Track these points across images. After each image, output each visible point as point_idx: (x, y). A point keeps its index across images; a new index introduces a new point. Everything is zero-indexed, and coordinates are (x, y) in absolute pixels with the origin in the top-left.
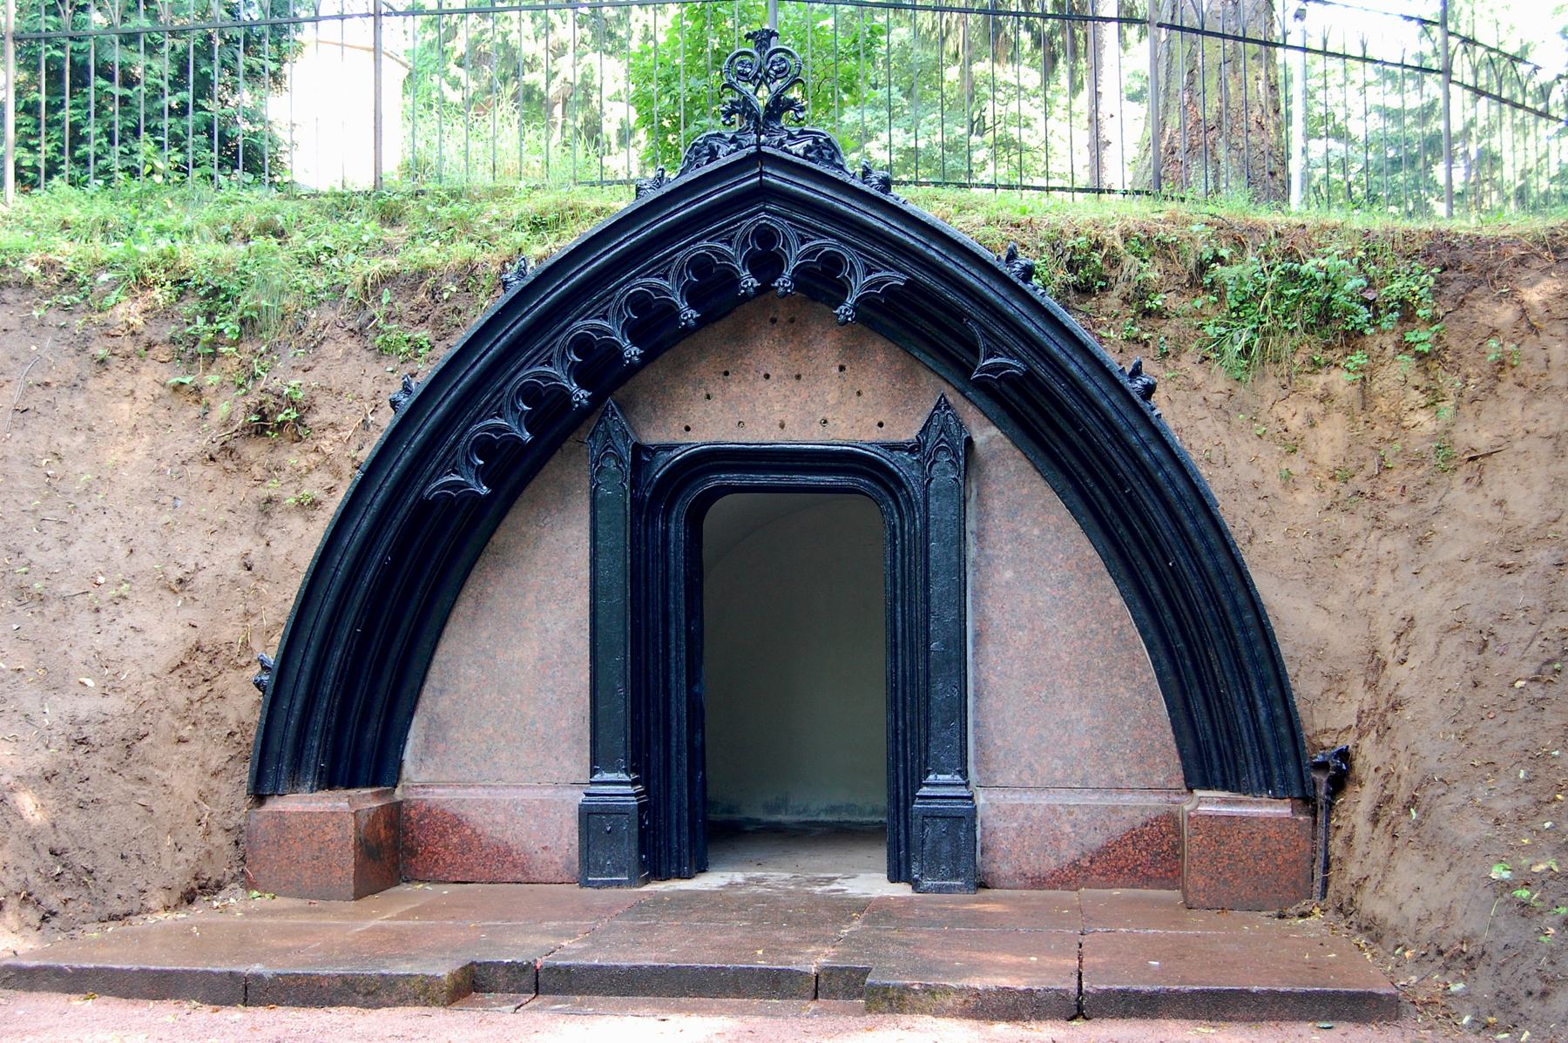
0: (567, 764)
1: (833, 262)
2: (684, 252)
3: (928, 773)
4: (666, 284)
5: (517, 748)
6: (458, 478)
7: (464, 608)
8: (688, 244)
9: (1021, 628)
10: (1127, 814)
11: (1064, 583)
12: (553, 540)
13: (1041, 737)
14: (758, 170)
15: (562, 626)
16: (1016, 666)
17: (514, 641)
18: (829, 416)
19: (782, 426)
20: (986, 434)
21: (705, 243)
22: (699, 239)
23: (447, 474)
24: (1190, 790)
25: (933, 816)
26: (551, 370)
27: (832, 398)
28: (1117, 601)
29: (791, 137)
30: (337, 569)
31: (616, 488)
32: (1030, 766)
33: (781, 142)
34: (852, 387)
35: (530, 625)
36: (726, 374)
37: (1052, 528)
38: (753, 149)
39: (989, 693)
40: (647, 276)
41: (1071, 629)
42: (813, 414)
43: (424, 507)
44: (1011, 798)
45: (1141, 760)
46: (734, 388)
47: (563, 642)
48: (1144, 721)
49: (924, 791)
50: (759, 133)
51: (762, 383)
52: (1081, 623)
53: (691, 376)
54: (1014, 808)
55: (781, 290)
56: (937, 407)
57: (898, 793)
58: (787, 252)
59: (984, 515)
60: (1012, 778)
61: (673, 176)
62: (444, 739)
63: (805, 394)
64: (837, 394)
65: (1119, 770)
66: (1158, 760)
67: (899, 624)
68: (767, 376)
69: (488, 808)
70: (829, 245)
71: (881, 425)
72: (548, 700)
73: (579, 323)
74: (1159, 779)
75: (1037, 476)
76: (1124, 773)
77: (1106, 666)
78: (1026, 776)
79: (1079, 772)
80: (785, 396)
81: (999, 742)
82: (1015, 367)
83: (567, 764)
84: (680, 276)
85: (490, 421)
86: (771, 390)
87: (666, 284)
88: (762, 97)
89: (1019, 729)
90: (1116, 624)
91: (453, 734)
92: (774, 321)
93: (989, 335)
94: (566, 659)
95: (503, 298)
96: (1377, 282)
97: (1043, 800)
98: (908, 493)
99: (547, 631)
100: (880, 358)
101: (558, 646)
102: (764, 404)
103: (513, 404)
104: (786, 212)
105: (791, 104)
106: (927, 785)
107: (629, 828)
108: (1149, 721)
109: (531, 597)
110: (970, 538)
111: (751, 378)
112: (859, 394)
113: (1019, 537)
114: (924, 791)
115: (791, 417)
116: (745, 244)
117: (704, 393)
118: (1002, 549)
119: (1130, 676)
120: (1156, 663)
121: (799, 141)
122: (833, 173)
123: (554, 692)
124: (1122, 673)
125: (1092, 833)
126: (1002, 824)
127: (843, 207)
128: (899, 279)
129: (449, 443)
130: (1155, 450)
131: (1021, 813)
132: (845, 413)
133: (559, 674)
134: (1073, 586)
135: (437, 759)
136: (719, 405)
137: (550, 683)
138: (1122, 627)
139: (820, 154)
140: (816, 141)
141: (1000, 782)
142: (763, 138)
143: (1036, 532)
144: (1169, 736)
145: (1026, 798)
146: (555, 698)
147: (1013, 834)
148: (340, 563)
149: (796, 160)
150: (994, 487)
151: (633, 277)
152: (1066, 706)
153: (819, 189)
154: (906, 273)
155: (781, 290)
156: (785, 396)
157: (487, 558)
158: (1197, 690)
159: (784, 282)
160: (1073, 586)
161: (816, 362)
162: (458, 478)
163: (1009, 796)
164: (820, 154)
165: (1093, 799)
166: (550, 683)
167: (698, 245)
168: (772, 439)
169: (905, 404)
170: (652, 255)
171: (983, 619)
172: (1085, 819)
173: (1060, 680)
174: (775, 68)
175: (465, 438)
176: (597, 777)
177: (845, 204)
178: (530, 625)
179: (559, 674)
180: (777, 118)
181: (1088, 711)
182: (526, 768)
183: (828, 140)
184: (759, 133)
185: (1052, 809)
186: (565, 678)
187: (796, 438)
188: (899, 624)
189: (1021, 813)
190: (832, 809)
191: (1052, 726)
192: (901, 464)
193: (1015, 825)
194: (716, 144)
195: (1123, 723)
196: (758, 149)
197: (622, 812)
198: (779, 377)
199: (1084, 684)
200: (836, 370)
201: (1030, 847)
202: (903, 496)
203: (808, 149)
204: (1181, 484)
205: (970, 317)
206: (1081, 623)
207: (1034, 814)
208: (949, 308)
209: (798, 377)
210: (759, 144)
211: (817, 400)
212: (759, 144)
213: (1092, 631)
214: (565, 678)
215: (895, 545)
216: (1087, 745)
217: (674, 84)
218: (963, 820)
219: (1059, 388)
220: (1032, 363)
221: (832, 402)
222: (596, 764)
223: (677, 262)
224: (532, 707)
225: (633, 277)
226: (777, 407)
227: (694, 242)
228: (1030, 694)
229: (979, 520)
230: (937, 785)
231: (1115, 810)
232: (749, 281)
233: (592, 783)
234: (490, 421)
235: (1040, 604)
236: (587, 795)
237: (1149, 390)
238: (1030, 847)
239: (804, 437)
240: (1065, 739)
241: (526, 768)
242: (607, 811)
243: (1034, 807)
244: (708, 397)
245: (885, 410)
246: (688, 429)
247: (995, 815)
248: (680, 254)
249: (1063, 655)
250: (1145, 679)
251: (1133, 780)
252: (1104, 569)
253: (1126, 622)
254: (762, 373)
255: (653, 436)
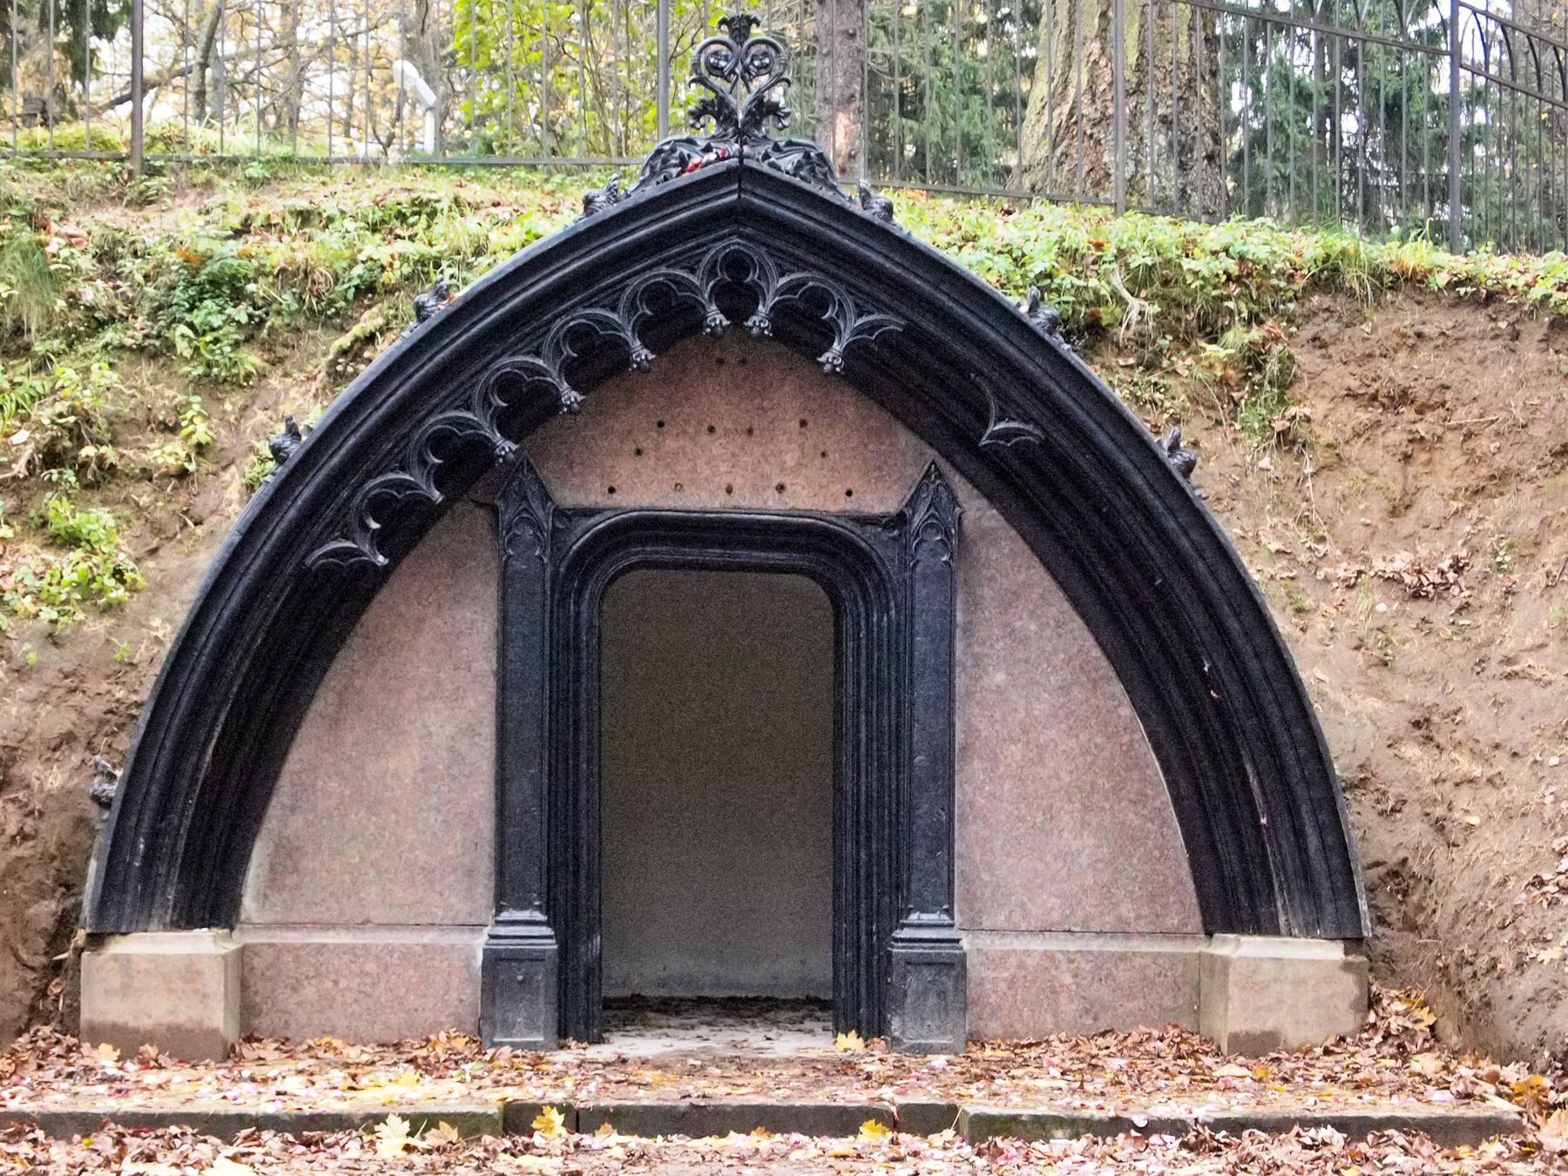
0: (453, 900)
1: (819, 300)
2: (638, 280)
3: (910, 911)
4: (614, 316)
5: (391, 880)
6: (349, 544)
7: (324, 703)
8: (644, 270)
9: (1013, 741)
10: (1138, 962)
11: (1064, 689)
12: (439, 622)
13: (1036, 872)
14: (735, 186)
15: (449, 730)
16: (1007, 787)
17: (388, 747)
18: (786, 481)
19: (729, 490)
20: (978, 512)
21: (663, 270)
22: (656, 264)
23: (335, 539)
24: (1210, 934)
25: (910, 963)
26: (470, 415)
27: (790, 459)
28: (1127, 711)
29: (777, 148)
30: (200, 654)
31: (533, 559)
32: (1023, 905)
33: (766, 156)
34: (815, 447)
35: (408, 728)
36: (661, 424)
37: (1052, 623)
38: (734, 162)
39: (975, 817)
40: (591, 306)
41: (1073, 743)
42: (768, 477)
43: (302, 573)
44: (998, 944)
45: (1152, 898)
46: (671, 444)
47: (451, 750)
48: (1156, 854)
49: (906, 933)
50: (743, 143)
51: (705, 438)
52: (1084, 737)
53: (617, 426)
54: (1005, 955)
55: (755, 331)
56: (927, 475)
57: (859, 939)
58: (763, 284)
59: (974, 604)
60: (1000, 920)
61: (631, 188)
62: (296, 870)
63: (758, 451)
64: (797, 454)
65: (1126, 910)
66: (1172, 899)
67: (863, 735)
68: (711, 430)
69: (355, 955)
70: (812, 279)
71: (849, 493)
72: (431, 821)
73: (506, 360)
74: (1173, 921)
75: (1035, 561)
76: (1132, 915)
77: (1113, 788)
78: (1016, 917)
79: (1080, 914)
80: (734, 455)
81: (986, 877)
82: (1030, 433)
83: (453, 900)
84: (633, 307)
85: (391, 476)
86: (716, 447)
87: (614, 316)
88: (741, 103)
89: (1011, 861)
90: (1126, 739)
91: (308, 863)
92: (720, 362)
93: (1003, 397)
94: (455, 771)
95: (422, 329)
96: (574, 153)
97: (1039, 945)
98: (880, 574)
99: (430, 734)
100: (850, 412)
101: (444, 754)
102: (707, 463)
103: (420, 454)
104: (762, 237)
105: (773, 109)
106: (910, 926)
107: (543, 978)
108: (1162, 853)
109: (411, 694)
110: (959, 633)
111: (691, 430)
112: (824, 454)
113: (1012, 633)
114: (906, 933)
115: (740, 480)
116: (711, 273)
117: (634, 447)
118: (992, 646)
119: (1141, 799)
120: (1172, 785)
121: (787, 154)
122: (827, 194)
123: (438, 811)
124: (1132, 796)
125: (1096, 985)
126: (991, 974)
127: (835, 236)
128: (895, 324)
129: (339, 501)
130: (1194, 535)
131: (1013, 961)
132: (807, 477)
133: (445, 789)
134: (1076, 692)
135: (285, 895)
136: (652, 462)
137: (434, 800)
138: (1132, 741)
139: (812, 170)
140: (807, 156)
141: (986, 924)
142: (746, 149)
143: (1033, 627)
144: (1185, 870)
145: (1020, 944)
146: (440, 818)
147: (1003, 986)
148: (205, 646)
149: (786, 177)
150: (984, 572)
151: (573, 307)
152: (1066, 834)
153: (809, 212)
154: (904, 317)
155: (755, 331)
156: (734, 455)
157: (356, 640)
158: (1222, 816)
159: (759, 319)
160: (1076, 692)
161: (771, 414)
162: (349, 544)
163: (997, 942)
164: (812, 170)
165: (1096, 945)
166: (434, 800)
167: (655, 271)
168: (717, 505)
169: (879, 468)
170: (598, 281)
171: (971, 730)
172: (1088, 967)
173: (1059, 804)
174: (757, 63)
175: (359, 496)
176: (505, 916)
177: (838, 231)
178: (408, 728)
179: (445, 789)
180: (758, 125)
181: (1091, 842)
182: (402, 906)
183: (820, 156)
184: (743, 143)
185: (1049, 956)
186: (453, 795)
187: (744, 504)
188: (863, 735)
189: (1013, 961)
190: (662, 983)
191: (1048, 858)
192: (877, 543)
193: (1006, 975)
194: (686, 152)
195: (1131, 856)
196: (741, 161)
197: (536, 958)
198: (726, 431)
199: (1086, 808)
200: (795, 425)
201: (1024, 1001)
202: (872, 580)
203: (799, 166)
204: (1224, 576)
205: (980, 373)
206: (1084, 737)
207: (1029, 962)
208: (953, 362)
209: (750, 431)
210: (741, 156)
211: (772, 460)
212: (741, 156)
213: (1096, 746)
214: (453, 795)
215: (859, 639)
216: (1089, 881)
217: (1501, 316)
218: (952, 966)
219: (1084, 461)
220: (1051, 429)
221: (790, 464)
222: (503, 896)
223: (628, 291)
224: (410, 830)
225: (573, 307)
226: (723, 468)
227: (650, 268)
228: (1021, 819)
229: (966, 611)
230: (920, 926)
231: (1123, 957)
232: (716, 317)
233: (498, 923)
234: (391, 476)
235: (1036, 713)
236: (492, 937)
237: (1188, 467)
238: (1024, 1001)
239: (756, 503)
240: (1064, 873)
241: (402, 906)
242: (516, 958)
243: (1027, 953)
244: (639, 452)
245: (855, 475)
246: (612, 490)
247: (982, 964)
248: (636, 281)
249: (1063, 774)
250: (1158, 804)
251: (1142, 922)
252: (1112, 674)
253: (1137, 736)
254: (706, 426)
255: (569, 497)
